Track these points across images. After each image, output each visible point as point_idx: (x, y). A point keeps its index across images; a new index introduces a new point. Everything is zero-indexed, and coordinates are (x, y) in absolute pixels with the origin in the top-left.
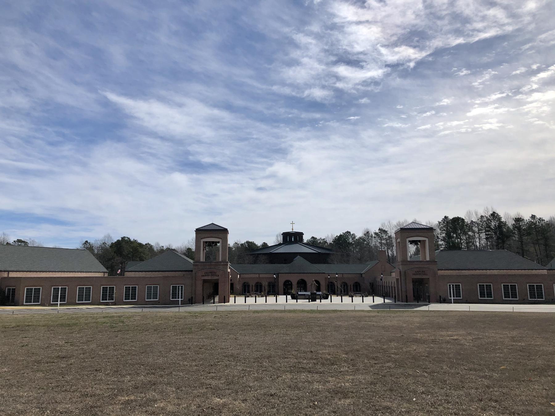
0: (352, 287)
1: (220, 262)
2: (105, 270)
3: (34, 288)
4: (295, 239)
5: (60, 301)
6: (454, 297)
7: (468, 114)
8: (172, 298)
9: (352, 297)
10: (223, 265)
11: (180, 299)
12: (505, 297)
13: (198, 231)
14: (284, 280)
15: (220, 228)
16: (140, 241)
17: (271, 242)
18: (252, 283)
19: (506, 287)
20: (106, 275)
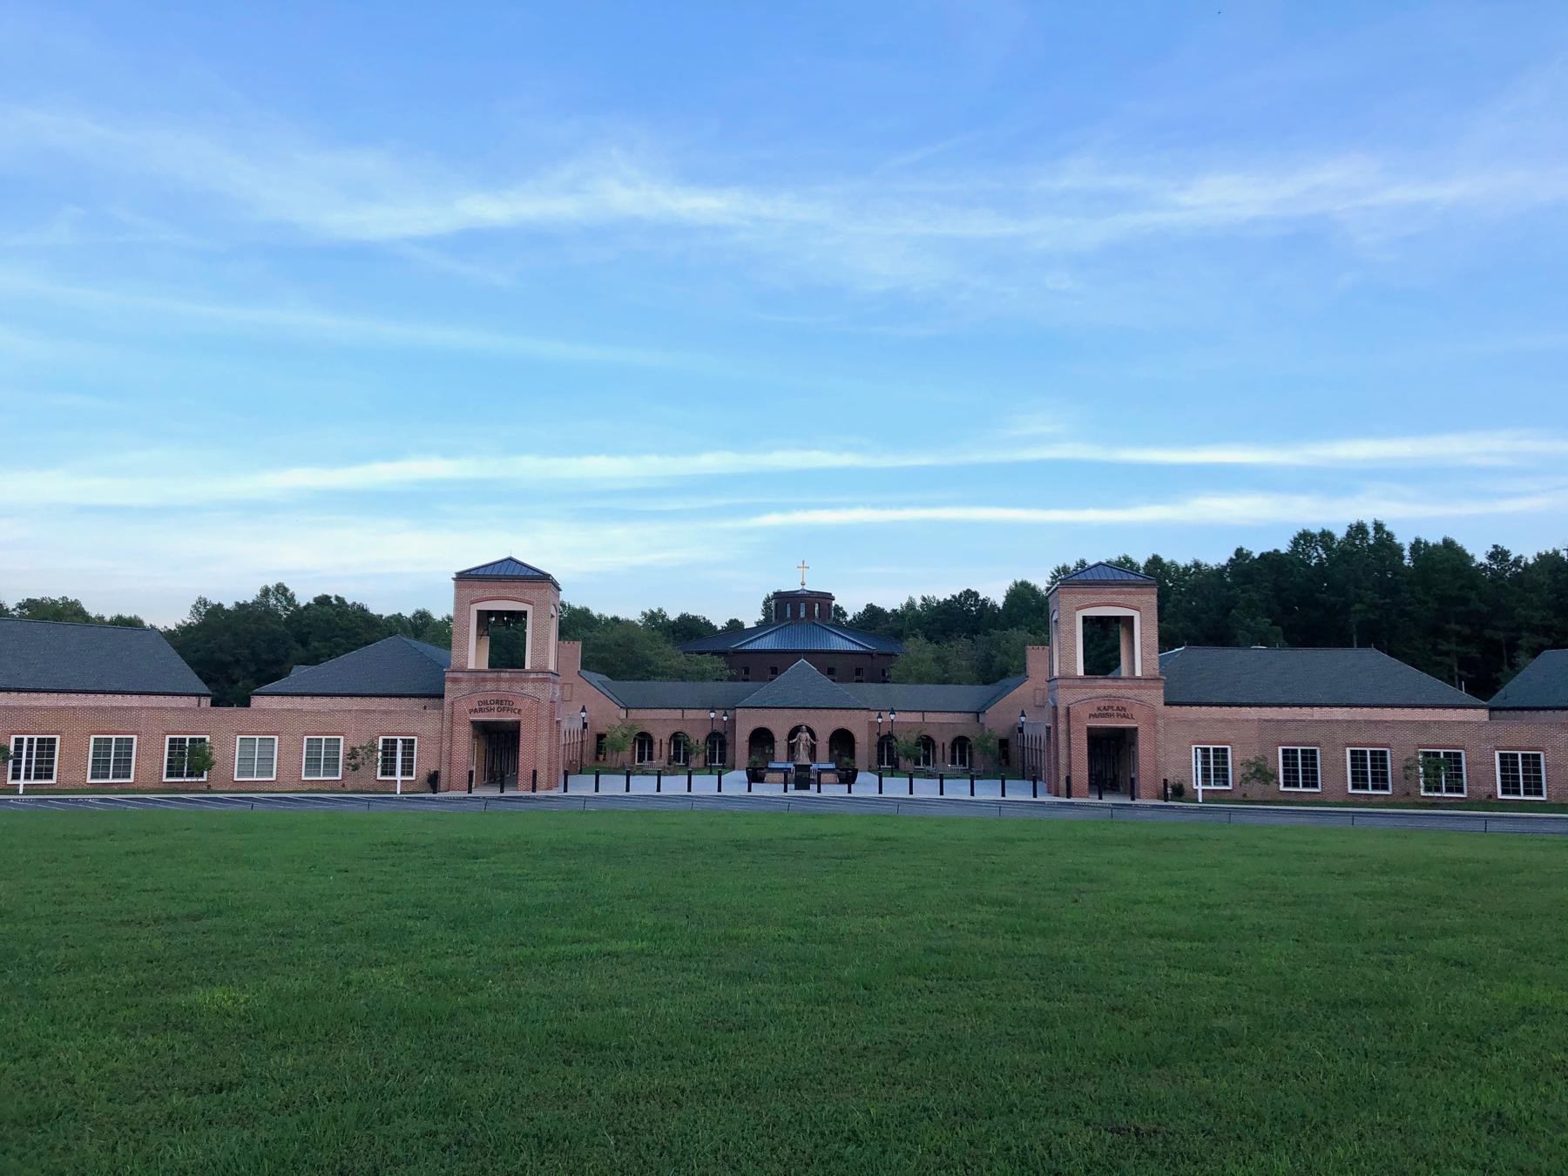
0: (948, 751)
1: (528, 672)
2: (205, 689)
3: (188, 737)
4: (810, 613)
5: (403, 774)
6: (27, 777)
7: (1186, 198)
8: (383, 774)
9: (628, 775)
10: (534, 680)
11: (399, 777)
12: (1354, 787)
13: (463, 578)
14: (750, 729)
15: (530, 573)
16: (375, 610)
17: (751, 617)
18: (943, 740)
19: (1358, 757)
20: (206, 702)
